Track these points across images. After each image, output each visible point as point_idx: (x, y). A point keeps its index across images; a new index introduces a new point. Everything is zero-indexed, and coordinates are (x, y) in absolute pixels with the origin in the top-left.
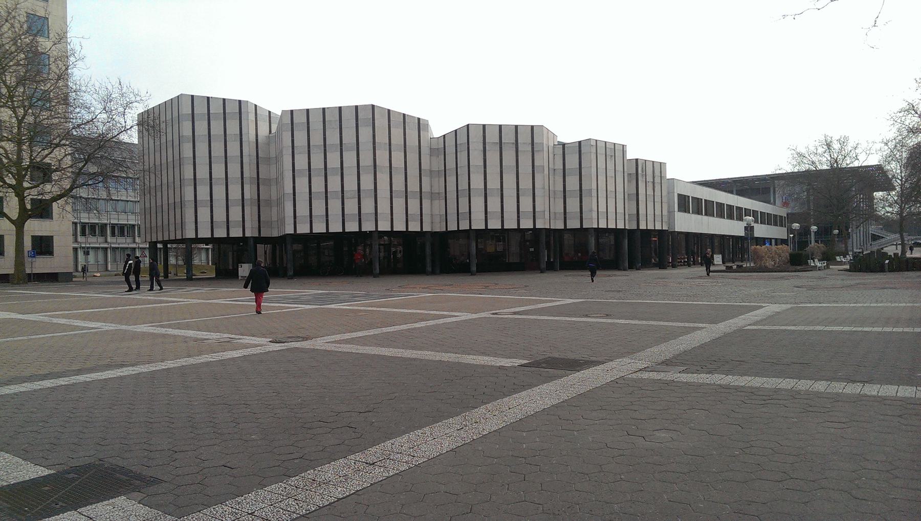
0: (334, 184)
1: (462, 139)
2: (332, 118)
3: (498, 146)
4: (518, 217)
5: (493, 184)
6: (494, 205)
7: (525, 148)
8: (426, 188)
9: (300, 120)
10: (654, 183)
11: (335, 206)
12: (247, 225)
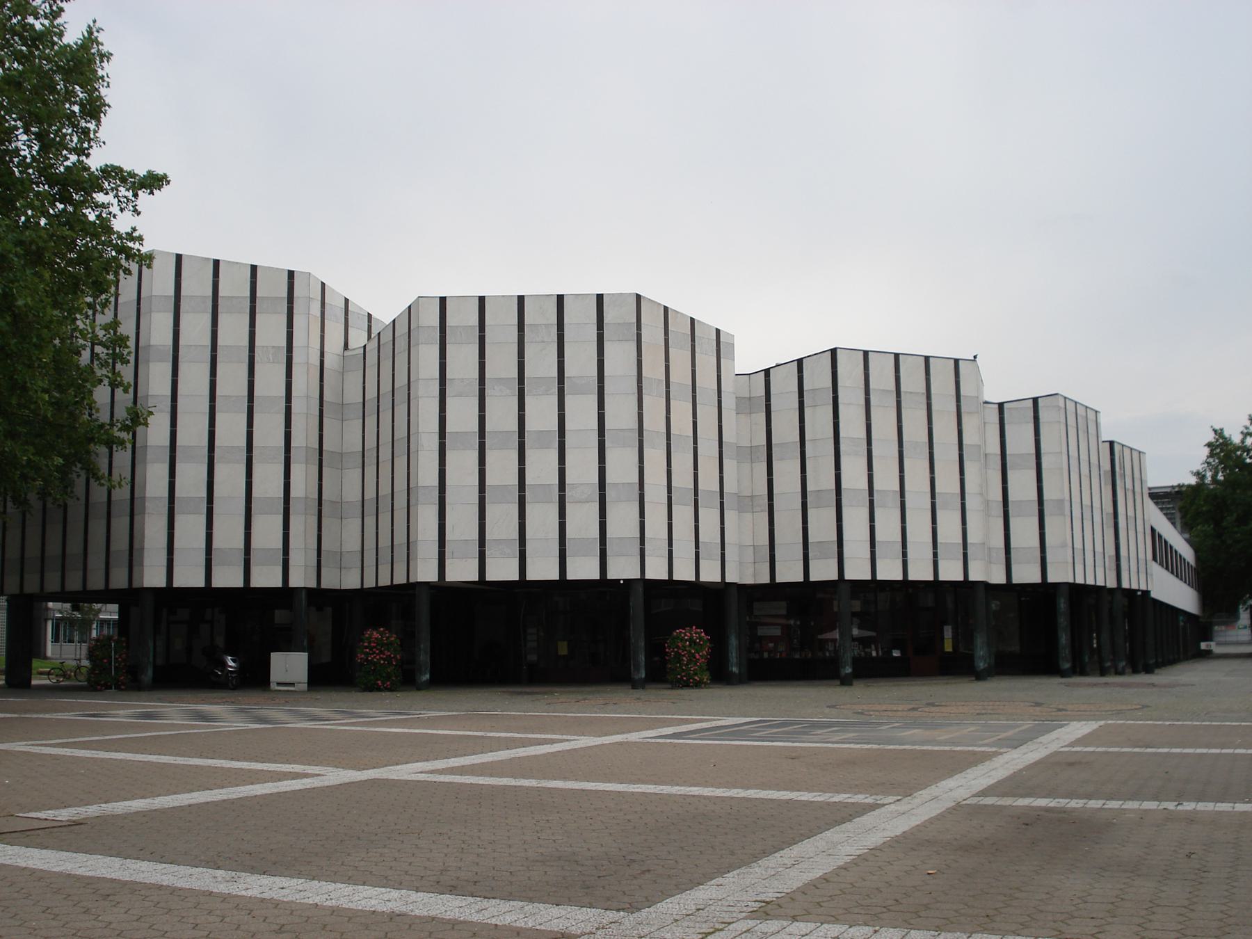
1: (818, 379)
2: (541, 319)
4: (935, 555)
5: (886, 481)
9: (462, 319)
11: (542, 519)
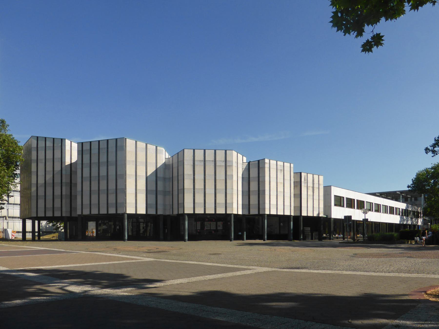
0: (103, 186)
2: (103, 146)
3: (213, 162)
4: (215, 206)
6: (199, 199)
7: (112, 149)
8: (160, 188)
10: (313, 187)
12: (159, 207)
